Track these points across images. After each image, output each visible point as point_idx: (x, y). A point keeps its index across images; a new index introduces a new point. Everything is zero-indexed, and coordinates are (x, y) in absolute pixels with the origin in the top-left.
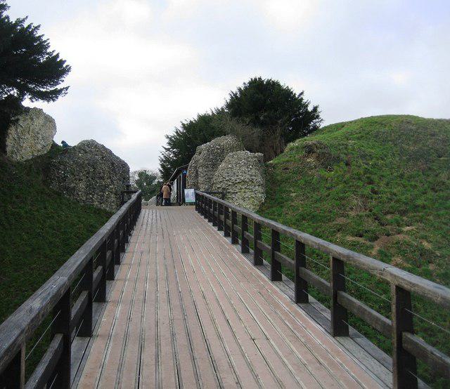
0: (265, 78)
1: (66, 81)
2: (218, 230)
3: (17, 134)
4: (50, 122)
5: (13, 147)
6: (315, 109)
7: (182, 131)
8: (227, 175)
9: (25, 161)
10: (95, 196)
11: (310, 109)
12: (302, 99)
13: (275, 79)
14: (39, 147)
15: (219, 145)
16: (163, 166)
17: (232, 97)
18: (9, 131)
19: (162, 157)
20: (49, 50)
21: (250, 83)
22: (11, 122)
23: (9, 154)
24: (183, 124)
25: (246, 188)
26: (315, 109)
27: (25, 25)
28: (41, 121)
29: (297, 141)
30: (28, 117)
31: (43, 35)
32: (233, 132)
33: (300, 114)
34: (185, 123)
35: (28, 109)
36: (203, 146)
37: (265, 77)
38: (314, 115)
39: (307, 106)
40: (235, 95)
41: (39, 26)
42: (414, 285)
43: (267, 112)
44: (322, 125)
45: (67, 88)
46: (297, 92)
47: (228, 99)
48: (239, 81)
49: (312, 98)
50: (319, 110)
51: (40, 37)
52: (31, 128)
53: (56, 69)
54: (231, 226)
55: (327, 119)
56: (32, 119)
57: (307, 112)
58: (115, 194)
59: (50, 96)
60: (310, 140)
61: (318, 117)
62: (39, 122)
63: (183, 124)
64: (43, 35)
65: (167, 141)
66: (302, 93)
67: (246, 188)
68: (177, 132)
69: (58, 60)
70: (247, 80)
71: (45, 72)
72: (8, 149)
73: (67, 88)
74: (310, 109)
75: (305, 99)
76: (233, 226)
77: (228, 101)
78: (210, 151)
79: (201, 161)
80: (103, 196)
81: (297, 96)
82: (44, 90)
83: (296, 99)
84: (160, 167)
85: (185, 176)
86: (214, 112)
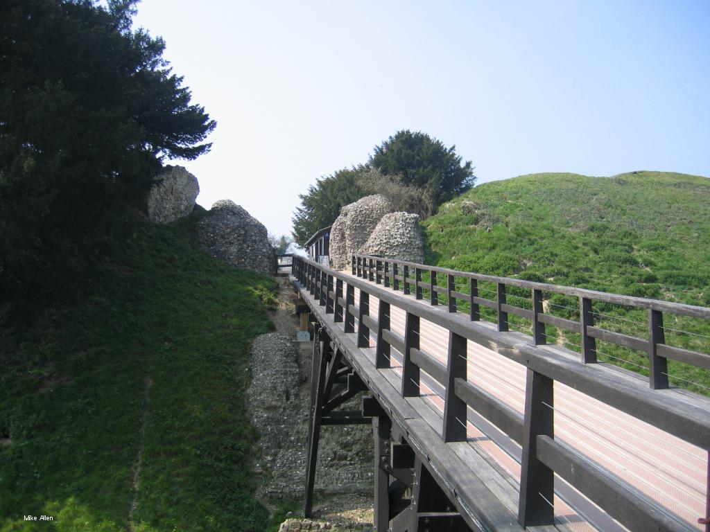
0: (413, 130)
1: (210, 137)
2: (405, 294)
3: (160, 194)
4: (192, 181)
5: (155, 208)
6: (468, 165)
7: (318, 189)
8: (384, 237)
9: (169, 223)
10: (248, 261)
11: (462, 165)
12: (454, 154)
13: (424, 132)
14: (183, 208)
15: (367, 206)
16: (296, 229)
17: (377, 152)
18: (151, 191)
19: (296, 218)
20: (190, 104)
21: (396, 137)
22: (154, 182)
23: (151, 217)
24: (319, 181)
25: (405, 251)
26: (468, 165)
27: (168, 77)
28: (185, 181)
29: (360, 201)
30: (171, 176)
31: (188, 88)
32: (383, 191)
33: (452, 171)
34: (321, 179)
35: (169, 167)
36: (349, 206)
37: (414, 130)
38: (466, 172)
39: (459, 162)
40: (381, 150)
41: (182, 78)
42: (573, 354)
43: (418, 167)
44: (477, 183)
45: (210, 145)
46: (447, 146)
47: (373, 154)
48: (383, 135)
49: (464, 155)
50: (472, 166)
51: (184, 89)
52: (174, 189)
53: (197, 123)
54: (326, 294)
55: (482, 175)
56: (175, 178)
57: (459, 169)
58: (268, 258)
59: (191, 154)
60: (467, 201)
61: (471, 173)
62: (181, 181)
63: (319, 181)
64: (188, 88)
65: (302, 200)
66: (453, 148)
67: (405, 251)
68: (312, 191)
69: (204, 114)
70: (393, 135)
71: (189, 126)
72: (151, 211)
73: (210, 145)
74: (462, 165)
75: (458, 153)
76: (328, 293)
77: (373, 157)
78: (359, 213)
79: (349, 223)
80: (256, 260)
81: (447, 151)
82: (183, 146)
83: (447, 154)
84: (293, 230)
85: (327, 239)
86: (357, 168)
